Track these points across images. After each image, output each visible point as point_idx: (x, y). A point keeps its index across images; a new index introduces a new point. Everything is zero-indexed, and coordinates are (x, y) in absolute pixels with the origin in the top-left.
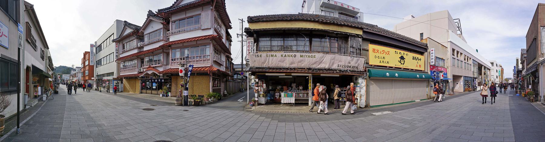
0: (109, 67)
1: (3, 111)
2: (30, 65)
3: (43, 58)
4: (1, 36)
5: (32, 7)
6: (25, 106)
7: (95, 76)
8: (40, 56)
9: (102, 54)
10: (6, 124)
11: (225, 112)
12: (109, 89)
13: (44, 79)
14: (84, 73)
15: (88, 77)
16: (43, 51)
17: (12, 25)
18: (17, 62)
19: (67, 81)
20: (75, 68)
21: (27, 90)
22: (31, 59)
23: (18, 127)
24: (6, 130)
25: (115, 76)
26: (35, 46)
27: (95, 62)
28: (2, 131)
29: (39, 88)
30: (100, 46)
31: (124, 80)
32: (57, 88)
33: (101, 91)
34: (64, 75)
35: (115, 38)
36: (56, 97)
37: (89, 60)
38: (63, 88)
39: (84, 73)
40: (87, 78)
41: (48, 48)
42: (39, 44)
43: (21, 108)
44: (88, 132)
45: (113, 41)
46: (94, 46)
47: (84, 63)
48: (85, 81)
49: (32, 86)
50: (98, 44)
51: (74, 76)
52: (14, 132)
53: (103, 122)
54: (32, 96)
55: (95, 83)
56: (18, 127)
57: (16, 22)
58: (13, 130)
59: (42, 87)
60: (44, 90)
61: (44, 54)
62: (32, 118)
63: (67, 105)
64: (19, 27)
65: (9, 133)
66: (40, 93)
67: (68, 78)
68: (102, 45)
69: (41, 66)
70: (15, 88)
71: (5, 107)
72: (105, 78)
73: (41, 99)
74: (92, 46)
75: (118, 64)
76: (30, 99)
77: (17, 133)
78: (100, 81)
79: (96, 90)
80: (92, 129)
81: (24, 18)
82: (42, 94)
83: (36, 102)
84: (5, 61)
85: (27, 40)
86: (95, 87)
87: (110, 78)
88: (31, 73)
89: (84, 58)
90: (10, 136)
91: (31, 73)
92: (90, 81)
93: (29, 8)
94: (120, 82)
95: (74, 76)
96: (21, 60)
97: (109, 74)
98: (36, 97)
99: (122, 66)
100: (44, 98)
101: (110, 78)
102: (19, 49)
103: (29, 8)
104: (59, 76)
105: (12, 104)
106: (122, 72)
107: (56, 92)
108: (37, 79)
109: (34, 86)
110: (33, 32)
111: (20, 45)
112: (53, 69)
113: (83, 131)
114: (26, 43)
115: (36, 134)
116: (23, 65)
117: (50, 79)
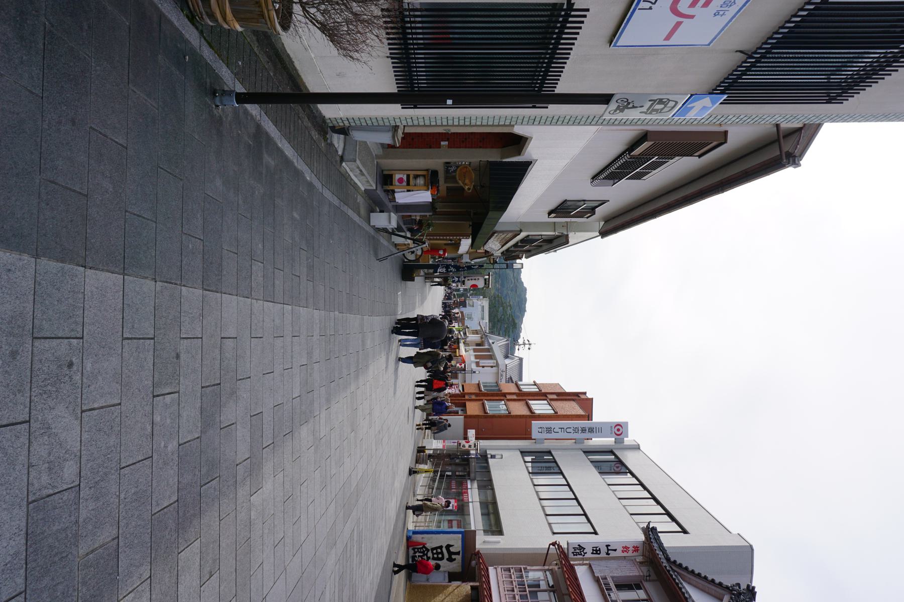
0: (525, 512)
1: (313, 20)
2: (531, 151)
3: (563, 209)
4: (674, 10)
5: (791, 158)
6: (343, 131)
7: (483, 443)
8: (572, 195)
9: (584, 478)
10: (251, 39)
11: (394, 500)
12: (418, 510)
13: (466, 215)
14: (497, 395)
15: (472, 417)
16: (592, 210)
17: (718, 65)
18: (546, 91)
19: (461, 320)
20: (520, 352)
21: (416, 141)
22: (559, 153)
23: (242, 98)
24: (218, 39)
25: (484, 542)
26: (615, 177)
27: (546, 445)
28: (212, 16)
29: (424, 196)
30: (620, 467)
31: (466, 588)
32: (428, 278)
33: (412, 472)
34: (485, 303)
35: (668, 541)
36: (388, 271)
37: (556, 416)
38: (430, 301)
39: (497, 395)
40: (473, 408)
41: (604, 233)
42: (626, 191)
43: (329, 111)
44: (229, 414)
45: (650, 532)
46: (619, 441)
47: (541, 395)
48: (460, 400)
49: (434, 160)
50: (629, 459)
51: (484, 352)
52: (218, 78)
53: (268, 486)
54: (390, 163)
55: (451, 444)
56: (242, 98)
57: (734, 86)
58: (225, 73)
59: (432, 206)
60: (417, 216)
61: (580, 215)
62: (287, 162)
63: (354, 320)
64: (707, 101)
65: (207, 53)
66: (403, 197)
67: (473, 324)
68: (628, 479)
69: (527, 204)
70: (422, 80)
71: (331, 32)
72: (473, 494)
73: (376, 204)
74: (619, 429)
75: (540, 559)
76: (377, 151)
77: (214, 91)
78: (458, 471)
79: (421, 450)
80: (242, 433)
81: (746, 122)
82: (399, 208)
83: (363, 180)
84: (552, 31)
85: (644, 137)
86: (435, 444)
87: (475, 519)
88: (492, 155)
89: (564, 396)
90: (198, 61)
91: (492, 155)
92: (456, 421)
93: (787, 147)
94: (455, 566)
95: (484, 352)
96: (554, 109)
97: (491, 510)
98: (386, 179)
99: (535, 575)
100: (381, 220)
101: (475, 519)
102: (605, 99)
103: (787, 147)
104: (480, 284)
105: (345, 66)
106: (494, 571)
107: (407, 272)
108: (468, 187)
109: (434, 174)
110: (680, 166)
111: (627, 104)
112: (511, 255)
113: (233, 393)
114: (626, 136)
115: (219, 182)
116: (533, 121)
117: (465, 244)
